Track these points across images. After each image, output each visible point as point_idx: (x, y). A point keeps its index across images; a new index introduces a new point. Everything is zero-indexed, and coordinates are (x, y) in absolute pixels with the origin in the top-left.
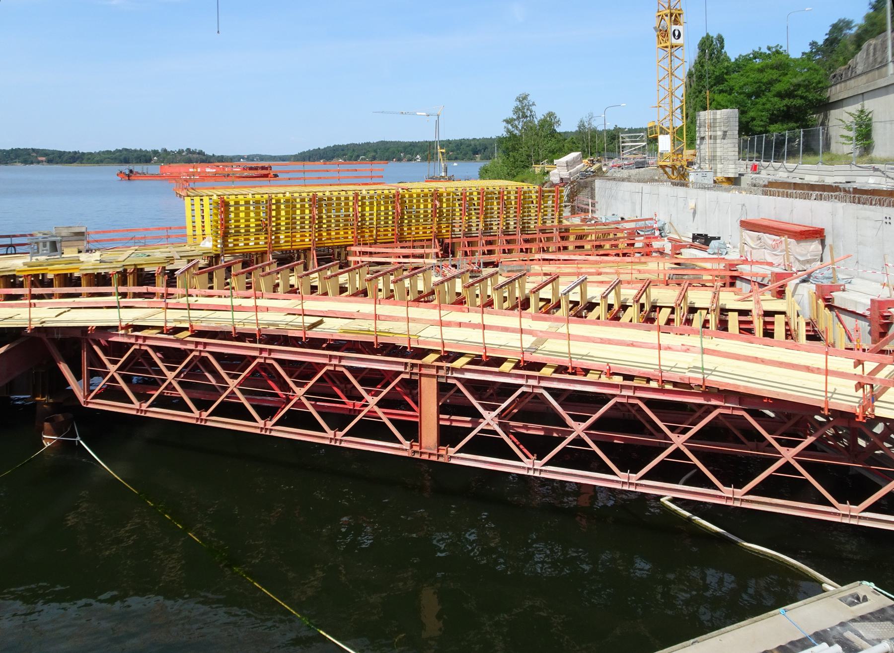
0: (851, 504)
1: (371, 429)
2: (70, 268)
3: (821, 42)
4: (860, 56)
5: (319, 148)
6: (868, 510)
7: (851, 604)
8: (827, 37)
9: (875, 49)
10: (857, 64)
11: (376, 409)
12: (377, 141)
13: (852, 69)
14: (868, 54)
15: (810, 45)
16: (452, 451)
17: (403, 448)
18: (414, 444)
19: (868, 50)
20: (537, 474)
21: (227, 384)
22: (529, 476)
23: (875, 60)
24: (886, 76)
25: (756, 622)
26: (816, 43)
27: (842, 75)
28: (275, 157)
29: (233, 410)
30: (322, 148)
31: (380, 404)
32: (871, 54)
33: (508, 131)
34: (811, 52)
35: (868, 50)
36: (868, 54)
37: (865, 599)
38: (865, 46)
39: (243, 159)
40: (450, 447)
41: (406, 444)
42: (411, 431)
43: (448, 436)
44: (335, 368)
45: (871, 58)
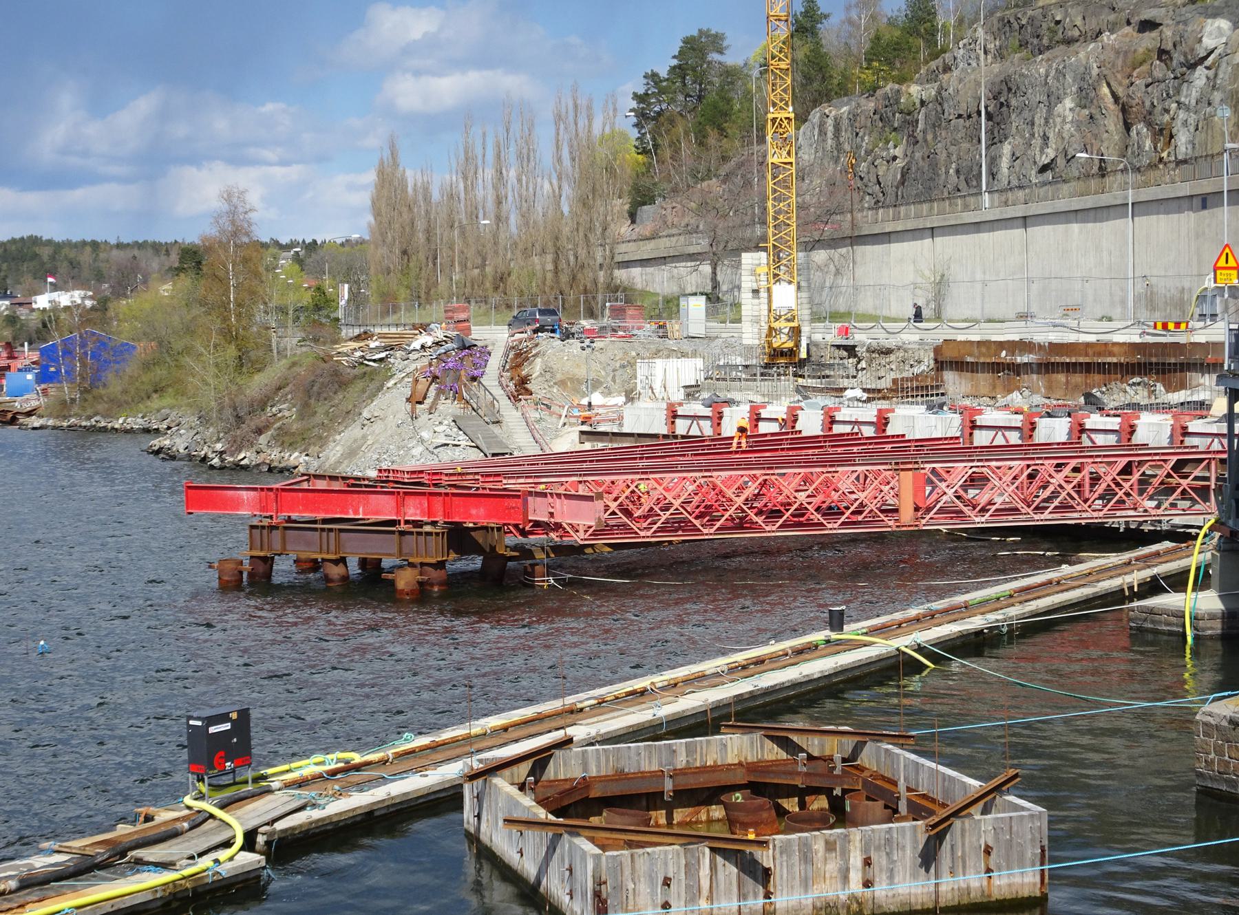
8: (675, 62)
24: (978, 208)
32: (830, 135)
34: (646, 94)
35: (822, 125)
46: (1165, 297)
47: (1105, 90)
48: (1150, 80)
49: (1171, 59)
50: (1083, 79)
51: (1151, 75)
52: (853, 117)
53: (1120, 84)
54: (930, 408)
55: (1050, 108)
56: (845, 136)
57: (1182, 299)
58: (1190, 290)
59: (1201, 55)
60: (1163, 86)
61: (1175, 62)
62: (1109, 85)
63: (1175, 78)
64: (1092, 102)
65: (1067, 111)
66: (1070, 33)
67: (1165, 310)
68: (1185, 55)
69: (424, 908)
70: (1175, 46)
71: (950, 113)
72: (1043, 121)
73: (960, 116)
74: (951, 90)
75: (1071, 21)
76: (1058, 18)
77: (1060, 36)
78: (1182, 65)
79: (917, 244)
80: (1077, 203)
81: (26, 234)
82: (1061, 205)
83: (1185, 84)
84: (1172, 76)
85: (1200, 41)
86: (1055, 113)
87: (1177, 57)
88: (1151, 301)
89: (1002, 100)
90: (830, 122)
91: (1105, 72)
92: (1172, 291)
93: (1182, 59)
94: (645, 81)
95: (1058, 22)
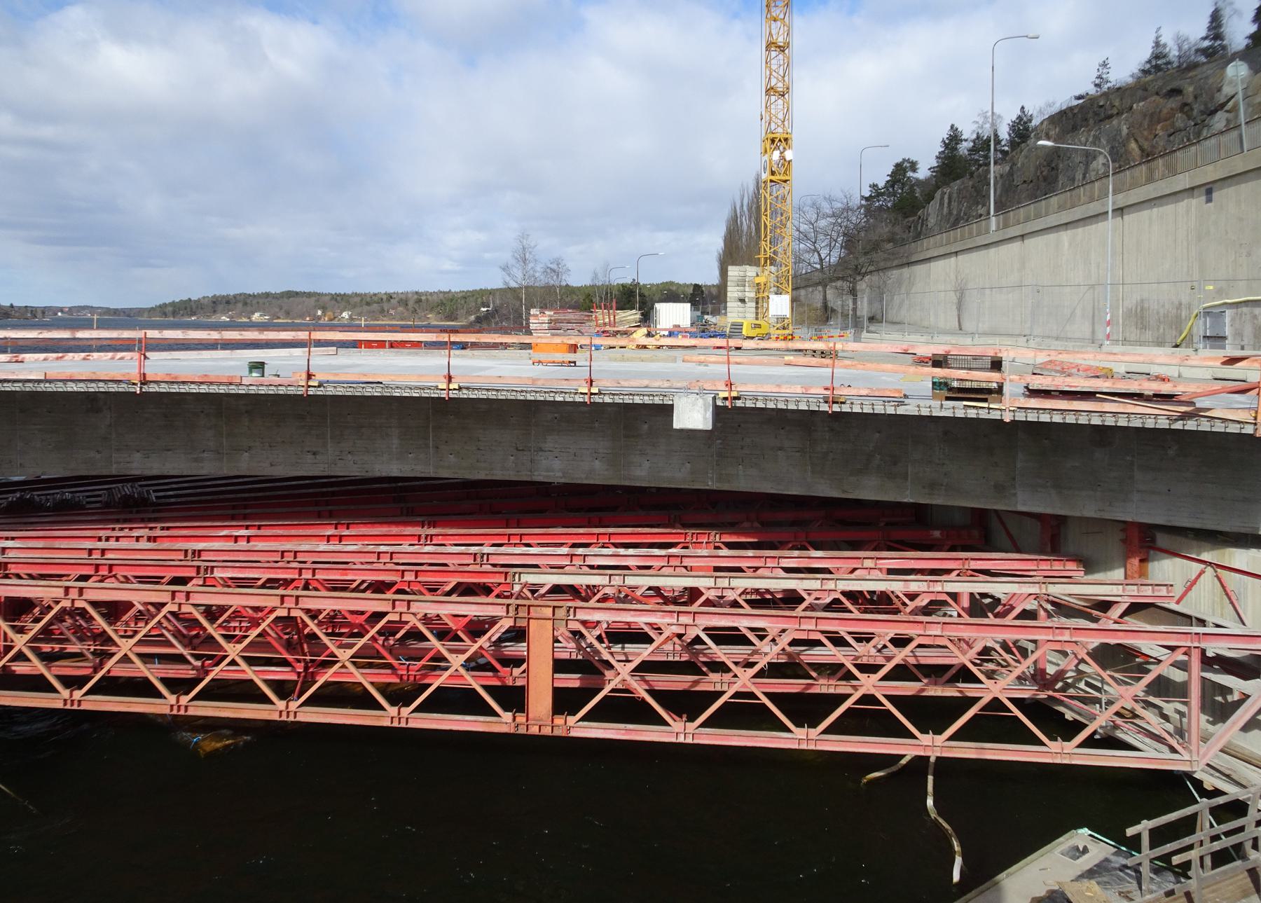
0: (1064, 740)
1: (464, 701)
2: (983, 557)
3: (881, 184)
4: (933, 207)
5: (190, 299)
6: (1080, 746)
7: (1075, 858)
8: (889, 178)
9: (950, 199)
10: (928, 215)
11: (462, 671)
12: (282, 291)
13: (923, 221)
14: (942, 204)
15: (870, 186)
16: (572, 720)
17: (503, 722)
18: (517, 714)
19: (942, 199)
20: (812, 747)
21: (226, 651)
22: (679, 743)
23: (950, 213)
24: (987, 231)
25: (982, 892)
26: (876, 185)
27: (910, 227)
28: (117, 310)
29: (464, 701)
30: (194, 298)
31: (468, 666)
32: (946, 205)
33: (506, 283)
34: (871, 196)
35: (942, 199)
36: (942, 204)
37: (1085, 850)
38: (938, 195)
39: (62, 311)
40: (569, 714)
41: (507, 716)
42: (514, 699)
43: (565, 702)
44: (289, 613)
45: (945, 210)
46: (1158, 313)
47: (1133, 145)
48: (1172, 130)
49: (1192, 109)
50: (1115, 140)
51: (1173, 125)
52: (960, 191)
53: (1146, 139)
54: (679, 326)
55: (1087, 165)
56: (954, 204)
57: (1178, 317)
58: (1189, 307)
59: (1221, 102)
60: (1183, 133)
61: (1195, 112)
62: (1136, 141)
63: (1195, 125)
64: (1121, 156)
65: (1100, 166)
66: (1110, 112)
67: (1158, 329)
68: (1206, 104)
69: (958, 861)
70: (1196, 97)
71: (1018, 180)
72: (1081, 176)
73: (1025, 182)
74: (1019, 165)
75: (1111, 103)
76: (1101, 104)
77: (1102, 115)
78: (1202, 113)
79: (947, 261)
80: (1065, 217)
81: (668, 281)
82: (1053, 220)
83: (1206, 128)
84: (1193, 124)
85: (1219, 90)
86: (1091, 168)
87: (1197, 108)
88: (1142, 317)
89: (1053, 165)
90: (946, 197)
91: (1135, 131)
92: (1167, 307)
93: (1202, 107)
94: (870, 189)
95: (1101, 106)
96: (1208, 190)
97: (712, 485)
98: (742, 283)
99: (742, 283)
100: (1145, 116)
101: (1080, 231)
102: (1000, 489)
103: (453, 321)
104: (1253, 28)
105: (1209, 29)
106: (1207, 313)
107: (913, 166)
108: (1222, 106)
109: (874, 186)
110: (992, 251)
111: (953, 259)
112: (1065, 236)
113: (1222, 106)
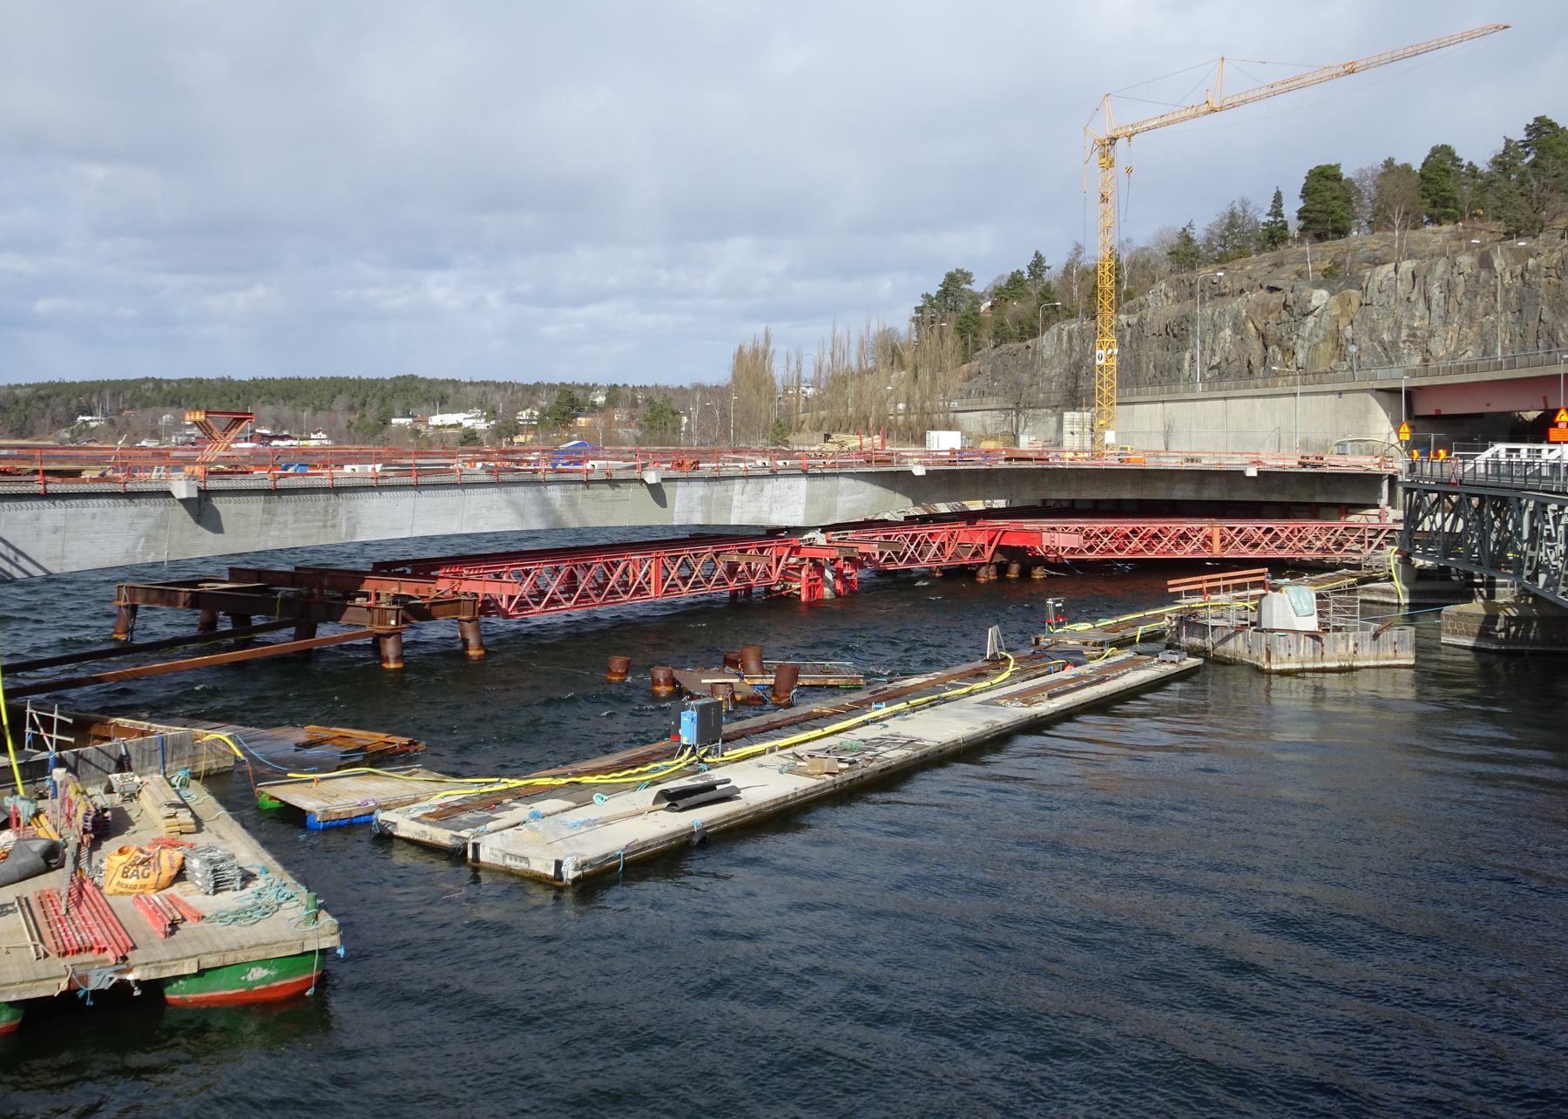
45: (1065, 345)
47: (1251, 325)
71: (1147, 332)
96: (1340, 393)
97: (1227, 498)
98: (1072, 423)
99: (1072, 423)
100: (1258, 305)
101: (1268, 400)
102: (1312, 496)
103: (24, 438)
104: (1301, 204)
105: (1273, 206)
106: (1338, 444)
107: (967, 277)
108: (1312, 312)
109: (927, 296)
110: (1199, 403)
111: (1160, 405)
112: (1258, 402)
113: (1312, 312)
